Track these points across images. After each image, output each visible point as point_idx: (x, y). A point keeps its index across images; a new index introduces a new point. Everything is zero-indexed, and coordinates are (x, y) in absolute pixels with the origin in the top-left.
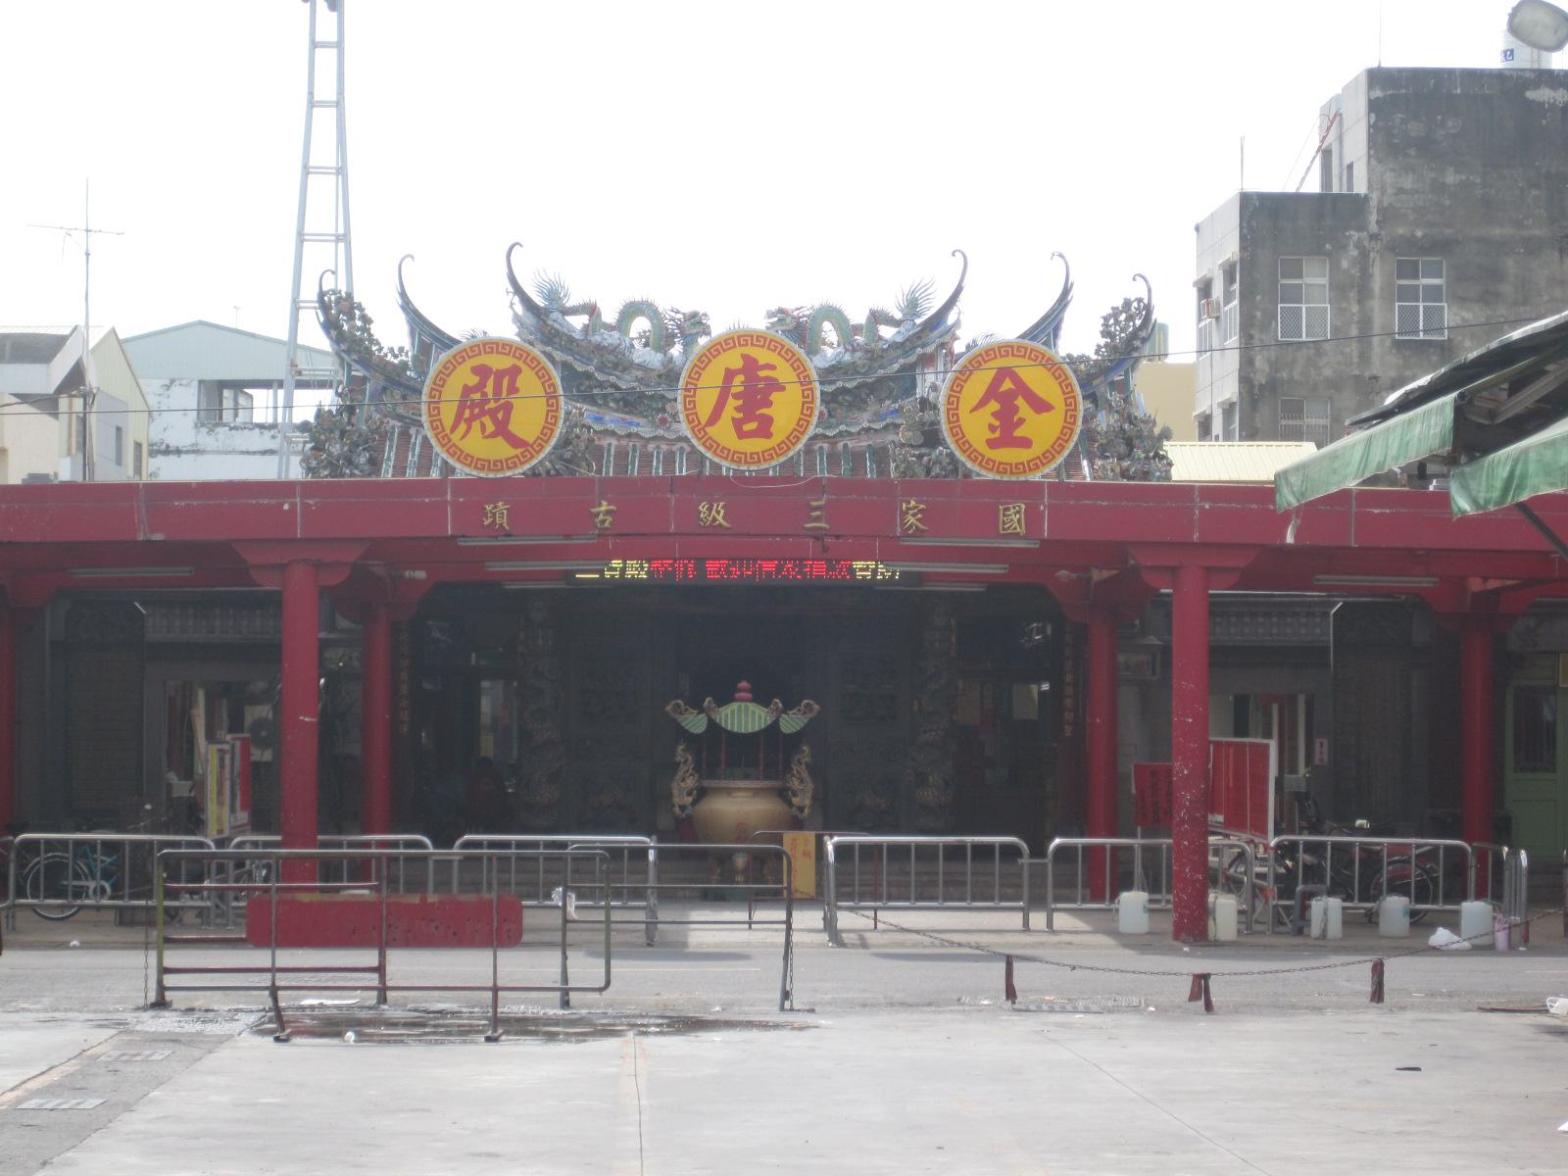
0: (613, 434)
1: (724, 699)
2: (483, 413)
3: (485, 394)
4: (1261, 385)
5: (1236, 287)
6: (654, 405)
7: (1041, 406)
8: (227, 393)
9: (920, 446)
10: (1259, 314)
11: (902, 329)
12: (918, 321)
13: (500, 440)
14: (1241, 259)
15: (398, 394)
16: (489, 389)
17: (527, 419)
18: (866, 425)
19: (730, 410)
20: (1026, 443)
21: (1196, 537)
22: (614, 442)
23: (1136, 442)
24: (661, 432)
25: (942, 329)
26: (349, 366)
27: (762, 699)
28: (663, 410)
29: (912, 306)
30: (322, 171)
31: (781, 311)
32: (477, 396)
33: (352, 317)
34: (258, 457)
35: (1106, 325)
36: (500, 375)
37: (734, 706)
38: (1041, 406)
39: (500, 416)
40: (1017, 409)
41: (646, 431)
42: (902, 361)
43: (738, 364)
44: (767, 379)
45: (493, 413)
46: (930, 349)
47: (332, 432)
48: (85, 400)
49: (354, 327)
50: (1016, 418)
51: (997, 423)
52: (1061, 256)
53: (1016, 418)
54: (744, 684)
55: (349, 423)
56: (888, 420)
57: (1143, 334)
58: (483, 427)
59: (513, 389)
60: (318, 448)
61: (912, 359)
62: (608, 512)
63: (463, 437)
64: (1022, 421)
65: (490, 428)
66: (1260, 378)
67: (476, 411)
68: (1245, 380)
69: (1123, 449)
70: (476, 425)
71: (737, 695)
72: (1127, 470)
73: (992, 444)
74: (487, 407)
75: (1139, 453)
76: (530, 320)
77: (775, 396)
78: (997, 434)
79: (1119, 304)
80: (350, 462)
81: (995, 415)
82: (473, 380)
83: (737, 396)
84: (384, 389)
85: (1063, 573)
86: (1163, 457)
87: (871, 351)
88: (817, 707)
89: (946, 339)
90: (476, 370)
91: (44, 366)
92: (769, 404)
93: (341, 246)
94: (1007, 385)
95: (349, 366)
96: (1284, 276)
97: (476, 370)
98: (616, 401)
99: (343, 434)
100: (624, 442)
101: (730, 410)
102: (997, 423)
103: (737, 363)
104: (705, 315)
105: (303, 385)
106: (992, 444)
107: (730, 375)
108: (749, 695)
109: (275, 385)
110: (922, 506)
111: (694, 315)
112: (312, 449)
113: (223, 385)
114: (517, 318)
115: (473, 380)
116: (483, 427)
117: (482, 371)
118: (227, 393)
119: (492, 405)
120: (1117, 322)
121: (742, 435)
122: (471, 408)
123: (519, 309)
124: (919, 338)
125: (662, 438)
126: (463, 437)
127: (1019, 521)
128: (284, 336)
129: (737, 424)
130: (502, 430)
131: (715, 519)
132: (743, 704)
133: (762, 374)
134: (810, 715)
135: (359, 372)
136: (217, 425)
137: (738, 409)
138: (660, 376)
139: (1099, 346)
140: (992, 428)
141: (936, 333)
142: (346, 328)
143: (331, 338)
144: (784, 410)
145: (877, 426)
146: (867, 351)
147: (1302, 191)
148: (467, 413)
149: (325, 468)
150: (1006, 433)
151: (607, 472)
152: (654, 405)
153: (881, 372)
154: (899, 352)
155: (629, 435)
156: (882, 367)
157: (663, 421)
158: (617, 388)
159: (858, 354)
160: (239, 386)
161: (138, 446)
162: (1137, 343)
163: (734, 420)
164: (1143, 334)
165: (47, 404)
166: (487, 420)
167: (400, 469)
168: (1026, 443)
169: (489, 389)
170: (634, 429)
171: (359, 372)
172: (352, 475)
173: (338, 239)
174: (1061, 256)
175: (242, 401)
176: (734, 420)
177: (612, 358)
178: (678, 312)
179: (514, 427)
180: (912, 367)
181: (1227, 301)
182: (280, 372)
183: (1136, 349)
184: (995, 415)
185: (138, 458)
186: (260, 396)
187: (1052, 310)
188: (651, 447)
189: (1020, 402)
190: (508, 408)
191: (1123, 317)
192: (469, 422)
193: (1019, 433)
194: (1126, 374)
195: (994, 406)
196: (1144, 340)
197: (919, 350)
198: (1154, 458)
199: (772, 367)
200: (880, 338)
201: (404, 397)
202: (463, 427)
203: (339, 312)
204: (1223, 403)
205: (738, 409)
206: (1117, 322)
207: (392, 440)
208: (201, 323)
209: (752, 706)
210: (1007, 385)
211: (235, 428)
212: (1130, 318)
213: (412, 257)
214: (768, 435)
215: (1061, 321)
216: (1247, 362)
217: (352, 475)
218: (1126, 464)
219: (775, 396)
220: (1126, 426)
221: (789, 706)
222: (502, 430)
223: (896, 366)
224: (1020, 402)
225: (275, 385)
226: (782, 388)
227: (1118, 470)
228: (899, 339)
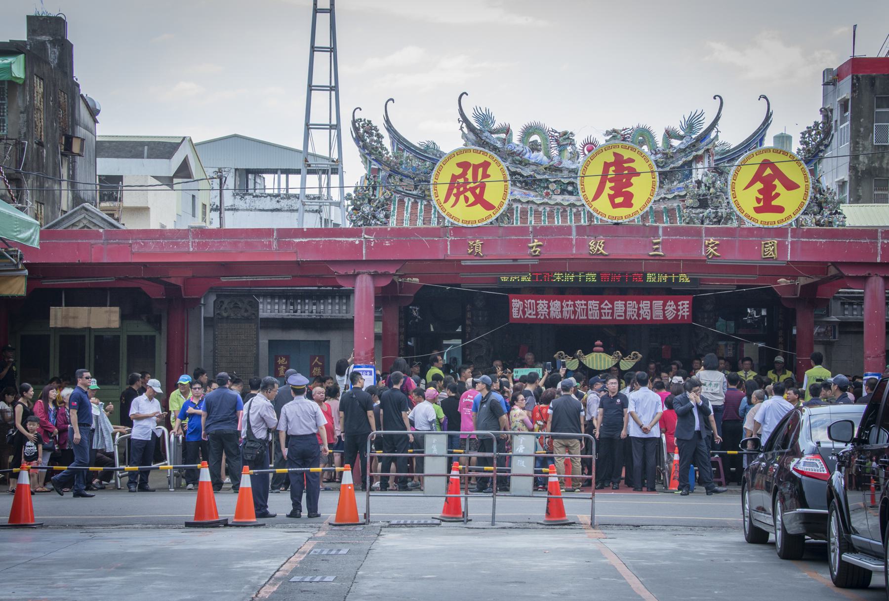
0: (519, 201)
1: (588, 351)
2: (466, 190)
3: (466, 180)
4: (862, 171)
5: (848, 114)
6: (542, 185)
7: (790, 186)
8: (250, 176)
9: (697, 208)
10: (862, 129)
11: (684, 141)
12: (693, 136)
13: (479, 206)
14: (852, 98)
15: (398, 177)
16: (469, 176)
17: (495, 193)
18: (663, 196)
19: (608, 191)
20: (780, 209)
21: (879, 260)
22: (520, 206)
23: (824, 205)
24: (546, 200)
25: (707, 141)
26: (370, 162)
27: (608, 351)
28: (548, 188)
29: (690, 126)
30: (322, 49)
31: (614, 131)
32: (461, 180)
33: (371, 135)
34: (270, 213)
35: (803, 137)
36: (476, 168)
37: (594, 355)
38: (790, 186)
39: (478, 191)
40: (775, 186)
41: (538, 200)
42: (684, 159)
43: (611, 159)
44: (629, 168)
45: (472, 190)
46: (700, 152)
47: (363, 199)
48: (221, 180)
49: (372, 140)
50: (773, 193)
51: (761, 197)
52: (765, 97)
53: (773, 193)
54: (599, 342)
55: (373, 195)
56: (676, 193)
57: (826, 142)
58: (467, 199)
59: (485, 175)
60: (356, 209)
61: (690, 158)
62: (538, 246)
63: (453, 206)
64: (778, 195)
65: (472, 199)
66: (862, 167)
67: (462, 189)
68: (853, 168)
69: (816, 209)
70: (462, 197)
71: (595, 349)
72: (819, 221)
73: (758, 210)
74: (468, 187)
75: (826, 212)
76: (472, 136)
77: (634, 180)
78: (762, 204)
79: (811, 125)
80: (374, 217)
81: (760, 191)
82: (459, 171)
83: (611, 181)
84: (390, 176)
85: (782, 280)
86: (840, 213)
87: (666, 154)
88: (640, 356)
89: (710, 146)
90: (459, 165)
91: (167, 161)
92: (631, 185)
93: (333, 93)
94: (768, 171)
95: (370, 162)
96: (878, 107)
97: (459, 165)
98: (520, 182)
99: (370, 201)
100: (524, 206)
101: (608, 191)
102: (761, 197)
103: (611, 159)
104: (571, 133)
105: (310, 172)
106: (758, 210)
107: (607, 166)
108: (601, 349)
109: (279, 172)
110: (717, 242)
111: (565, 133)
112: (353, 209)
113: (248, 171)
114: (464, 136)
115: (459, 171)
116: (467, 199)
117: (464, 165)
118: (250, 176)
119: (472, 185)
120: (810, 135)
121: (615, 206)
122: (456, 187)
123: (465, 130)
124: (694, 146)
125: (547, 204)
126: (453, 206)
127: (773, 251)
128: (300, 147)
129: (612, 198)
130: (480, 200)
131: (598, 250)
132: (598, 354)
133: (626, 165)
134: (636, 361)
135: (375, 166)
136: (245, 194)
137: (611, 188)
138: (546, 169)
139: (799, 149)
140: (758, 200)
141: (704, 143)
142: (368, 140)
143: (359, 147)
144: (643, 189)
145: (670, 196)
146: (664, 154)
147: (880, 56)
148: (455, 191)
149: (360, 220)
150: (767, 204)
151: (400, 220)
152: (542, 185)
153: (672, 166)
154: (683, 154)
155: (528, 202)
156: (672, 163)
157: (547, 194)
158: (522, 176)
159: (659, 155)
160: (258, 172)
161: (204, 206)
162: (822, 148)
163: (609, 195)
164: (826, 142)
165: (168, 181)
166: (468, 194)
167: (400, 220)
168: (780, 209)
169: (469, 176)
170: (531, 199)
171: (375, 166)
172: (376, 224)
173: (331, 89)
174: (765, 97)
175: (258, 180)
176: (609, 195)
177: (518, 158)
178: (556, 132)
179: (486, 197)
180: (691, 162)
181: (843, 121)
182: (299, 165)
183: (821, 151)
184: (760, 191)
185: (204, 213)
186: (269, 178)
187: (759, 129)
188: (541, 209)
189: (777, 182)
190: (483, 187)
191: (814, 133)
192: (457, 196)
193: (774, 203)
194: (815, 164)
195: (759, 185)
196: (826, 146)
197: (694, 153)
198: (835, 214)
199: (631, 160)
200: (672, 146)
201: (401, 180)
202: (453, 199)
203: (365, 132)
204: (838, 182)
205: (611, 188)
206: (810, 135)
207: (394, 205)
208: (235, 136)
209: (603, 355)
210: (768, 171)
211: (257, 196)
212: (818, 133)
213: (393, 100)
214: (630, 205)
215: (764, 135)
216: (854, 157)
217: (376, 224)
218: (818, 217)
219: (634, 180)
220: (818, 196)
221: (625, 354)
222: (480, 200)
223: (680, 163)
224: (777, 182)
225: (279, 172)
226: (638, 174)
227: (814, 221)
228: (683, 147)
